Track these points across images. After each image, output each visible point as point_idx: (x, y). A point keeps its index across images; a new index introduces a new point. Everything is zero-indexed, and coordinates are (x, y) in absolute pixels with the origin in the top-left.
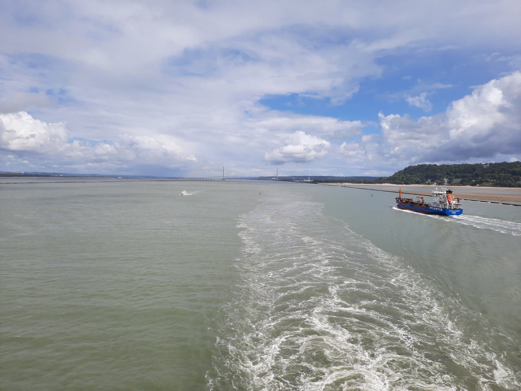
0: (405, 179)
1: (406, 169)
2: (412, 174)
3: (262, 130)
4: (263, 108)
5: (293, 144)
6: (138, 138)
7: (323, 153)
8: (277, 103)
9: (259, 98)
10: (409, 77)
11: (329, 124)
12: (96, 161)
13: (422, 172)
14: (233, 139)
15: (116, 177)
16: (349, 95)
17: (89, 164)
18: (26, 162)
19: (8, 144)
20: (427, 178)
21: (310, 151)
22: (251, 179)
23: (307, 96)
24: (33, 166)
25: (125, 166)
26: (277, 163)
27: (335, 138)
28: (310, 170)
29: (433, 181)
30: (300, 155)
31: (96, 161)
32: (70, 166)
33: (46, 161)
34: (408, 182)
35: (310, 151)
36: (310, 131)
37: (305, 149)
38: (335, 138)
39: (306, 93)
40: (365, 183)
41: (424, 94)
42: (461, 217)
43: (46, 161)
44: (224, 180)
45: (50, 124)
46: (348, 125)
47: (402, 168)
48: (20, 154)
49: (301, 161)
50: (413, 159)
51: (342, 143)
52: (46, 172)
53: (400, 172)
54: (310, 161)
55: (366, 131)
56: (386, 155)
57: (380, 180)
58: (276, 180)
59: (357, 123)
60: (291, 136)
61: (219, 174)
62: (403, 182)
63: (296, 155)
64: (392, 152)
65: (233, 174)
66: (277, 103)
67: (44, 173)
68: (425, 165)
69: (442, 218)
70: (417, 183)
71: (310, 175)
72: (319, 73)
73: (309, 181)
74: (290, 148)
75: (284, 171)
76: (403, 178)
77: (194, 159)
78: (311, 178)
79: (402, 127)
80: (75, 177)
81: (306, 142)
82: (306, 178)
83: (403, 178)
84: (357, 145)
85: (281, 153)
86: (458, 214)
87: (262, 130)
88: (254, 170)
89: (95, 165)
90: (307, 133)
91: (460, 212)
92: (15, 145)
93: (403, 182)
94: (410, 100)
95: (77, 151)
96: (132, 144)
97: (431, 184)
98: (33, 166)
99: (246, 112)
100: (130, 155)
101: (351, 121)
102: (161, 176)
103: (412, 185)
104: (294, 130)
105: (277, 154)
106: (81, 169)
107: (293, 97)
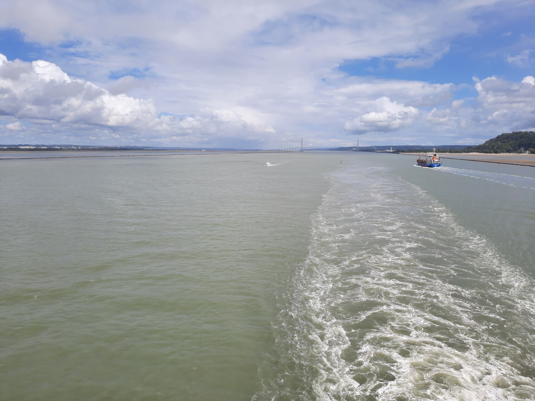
0: (495, 148)
1: (498, 137)
2: (504, 142)
3: (340, 98)
4: (342, 75)
5: (377, 112)
6: (216, 112)
7: (409, 121)
8: (357, 69)
9: (338, 65)
10: (509, 34)
11: (415, 88)
12: (180, 135)
13: (516, 140)
14: (310, 109)
15: (200, 150)
16: (438, 56)
17: (174, 138)
18: (117, 136)
19: (108, 120)
20: (520, 146)
21: (395, 119)
22: (330, 150)
23: (390, 59)
24: (123, 140)
25: (206, 139)
26: (359, 132)
27: (424, 104)
28: (394, 139)
29: (526, 150)
30: (385, 124)
31: (180, 135)
32: (156, 140)
33: (136, 136)
34: (498, 150)
35: (395, 119)
36: (395, 97)
37: (389, 117)
38: (424, 104)
39: (389, 57)
40: (451, 152)
41: (527, 52)
42: (439, 168)
43: (136, 136)
44: (302, 151)
45: (142, 100)
46: (440, 88)
47: (495, 136)
48: (114, 129)
49: (384, 129)
50: (515, 124)
51: (432, 109)
52: (423, 145)
53: (491, 140)
54: (395, 130)
55: (458, 95)
56: (482, 122)
57: (469, 149)
58: (356, 151)
59: (447, 86)
60: (373, 102)
61: (298, 145)
62: (492, 151)
63: (380, 124)
64: (490, 118)
65: (311, 145)
66: (357, 69)
67: (420, 146)
68: (521, 132)
69: (430, 168)
70: (508, 151)
71: (394, 145)
72: (403, 34)
73: (391, 151)
74: (372, 116)
75: (365, 141)
76: (493, 147)
77: (272, 130)
78: (394, 147)
79: (496, 90)
80: (164, 150)
81: (390, 108)
82: (389, 148)
83: (493, 147)
84: (448, 111)
85: (361, 122)
86: (438, 166)
87: (340, 98)
88: (332, 140)
89: (179, 138)
90: (392, 101)
91: (439, 165)
92: (112, 121)
93: (492, 151)
94: (510, 59)
95: (164, 125)
96: (213, 117)
97: (523, 153)
98: (123, 140)
99: (324, 80)
100: (213, 129)
101: (442, 83)
102: (241, 147)
103: (502, 154)
104: (377, 96)
105: (357, 124)
106: (166, 143)
107: (374, 62)
